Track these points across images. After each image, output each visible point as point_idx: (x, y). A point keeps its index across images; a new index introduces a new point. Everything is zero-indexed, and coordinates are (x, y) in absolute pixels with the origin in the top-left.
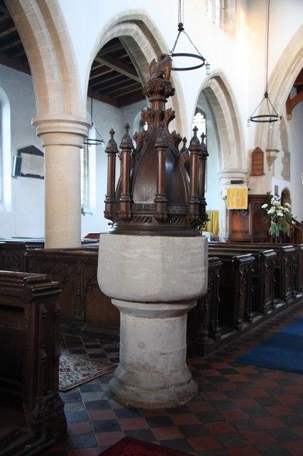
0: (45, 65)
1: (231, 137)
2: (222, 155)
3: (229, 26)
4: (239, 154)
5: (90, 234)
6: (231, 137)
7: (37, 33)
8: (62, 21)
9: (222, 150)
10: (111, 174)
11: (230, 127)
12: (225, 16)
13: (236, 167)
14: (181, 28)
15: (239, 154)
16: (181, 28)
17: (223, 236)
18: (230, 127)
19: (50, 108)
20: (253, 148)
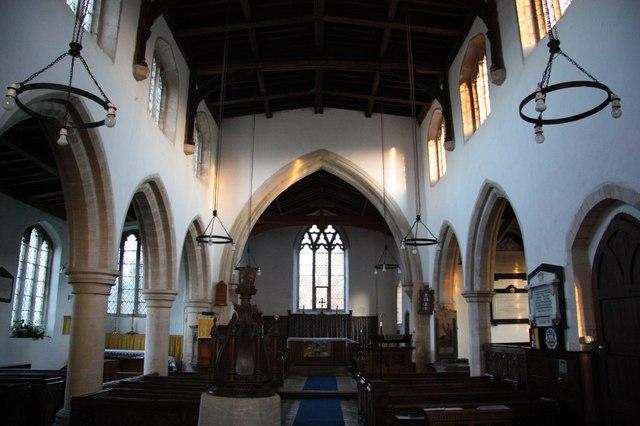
0: (90, 224)
1: (200, 271)
2: (190, 286)
3: (204, 178)
4: (205, 286)
5: (543, 265)
6: (200, 271)
7: (88, 199)
8: (111, 191)
9: (190, 282)
10: (560, 305)
11: (199, 262)
12: (201, 170)
13: (203, 297)
14: (215, 213)
15: (205, 286)
16: (215, 213)
17: (456, 277)
18: (199, 262)
19: (89, 262)
20: (217, 281)
